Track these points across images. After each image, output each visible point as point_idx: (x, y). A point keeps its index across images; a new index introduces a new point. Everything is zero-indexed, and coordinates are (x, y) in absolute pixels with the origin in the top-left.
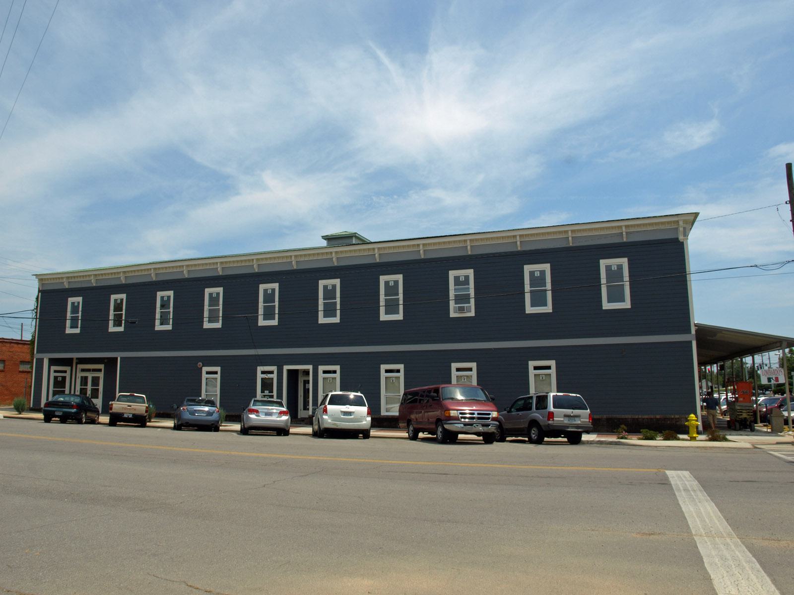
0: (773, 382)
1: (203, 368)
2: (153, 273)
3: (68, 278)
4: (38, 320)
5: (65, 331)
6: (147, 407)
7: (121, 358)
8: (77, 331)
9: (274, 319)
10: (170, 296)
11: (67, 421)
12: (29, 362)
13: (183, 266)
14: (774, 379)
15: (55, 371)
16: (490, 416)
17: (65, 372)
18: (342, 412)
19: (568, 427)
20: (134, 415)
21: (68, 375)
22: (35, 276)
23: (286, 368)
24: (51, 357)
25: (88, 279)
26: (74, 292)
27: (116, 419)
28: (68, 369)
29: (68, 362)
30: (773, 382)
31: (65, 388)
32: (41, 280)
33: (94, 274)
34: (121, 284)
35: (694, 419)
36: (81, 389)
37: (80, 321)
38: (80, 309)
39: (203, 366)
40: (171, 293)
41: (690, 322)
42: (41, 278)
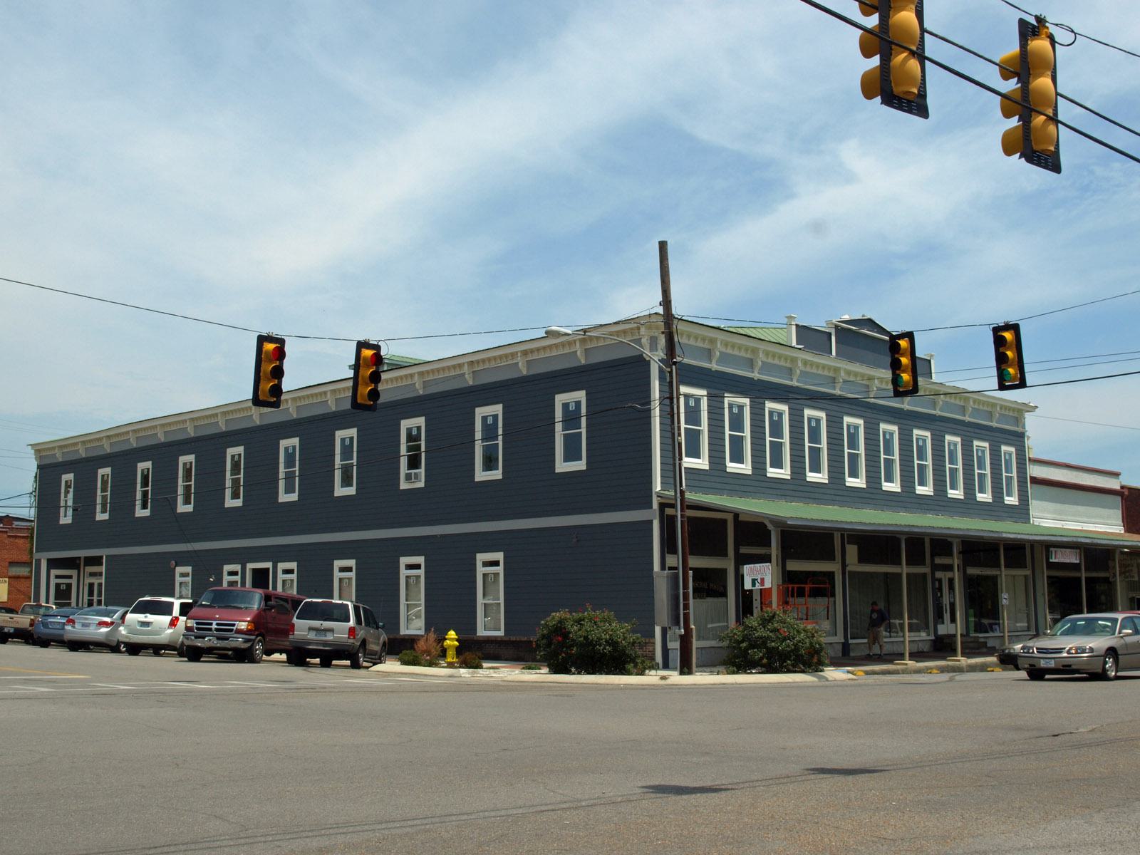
0: (758, 586)
1: (177, 568)
2: (579, 350)
3: (525, 353)
4: (62, 503)
5: (95, 517)
6: (31, 620)
7: (107, 556)
8: (581, 465)
9: (581, 459)
10: (353, 437)
11: (140, 652)
12: (27, 563)
13: (186, 421)
14: (759, 581)
15: (57, 577)
16: (235, 628)
17: (70, 577)
18: (139, 622)
19: (309, 644)
20: (16, 629)
21: (74, 582)
22: (30, 447)
23: (250, 566)
24: (51, 557)
25: (567, 350)
26: (485, 393)
27: (299, 656)
28: (74, 573)
29: (71, 563)
30: (758, 586)
31: (70, 599)
32: (38, 451)
33: (331, 390)
34: (132, 449)
35: (453, 637)
36: (89, 600)
37: (297, 478)
38: (500, 432)
39: (176, 566)
40: (581, 395)
41: (651, 489)
42: (39, 450)
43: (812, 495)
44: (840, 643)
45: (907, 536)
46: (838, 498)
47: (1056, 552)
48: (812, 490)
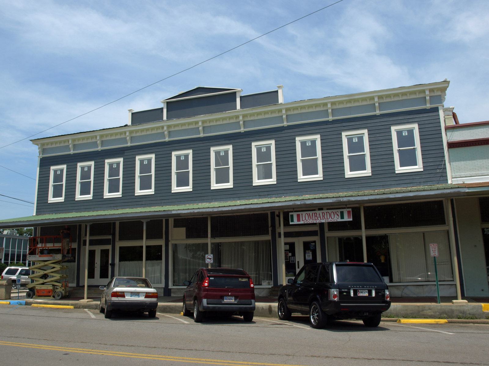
43: (140, 203)
44: (162, 288)
45: (92, 223)
46: (163, 201)
47: (302, 214)
48: (139, 200)
